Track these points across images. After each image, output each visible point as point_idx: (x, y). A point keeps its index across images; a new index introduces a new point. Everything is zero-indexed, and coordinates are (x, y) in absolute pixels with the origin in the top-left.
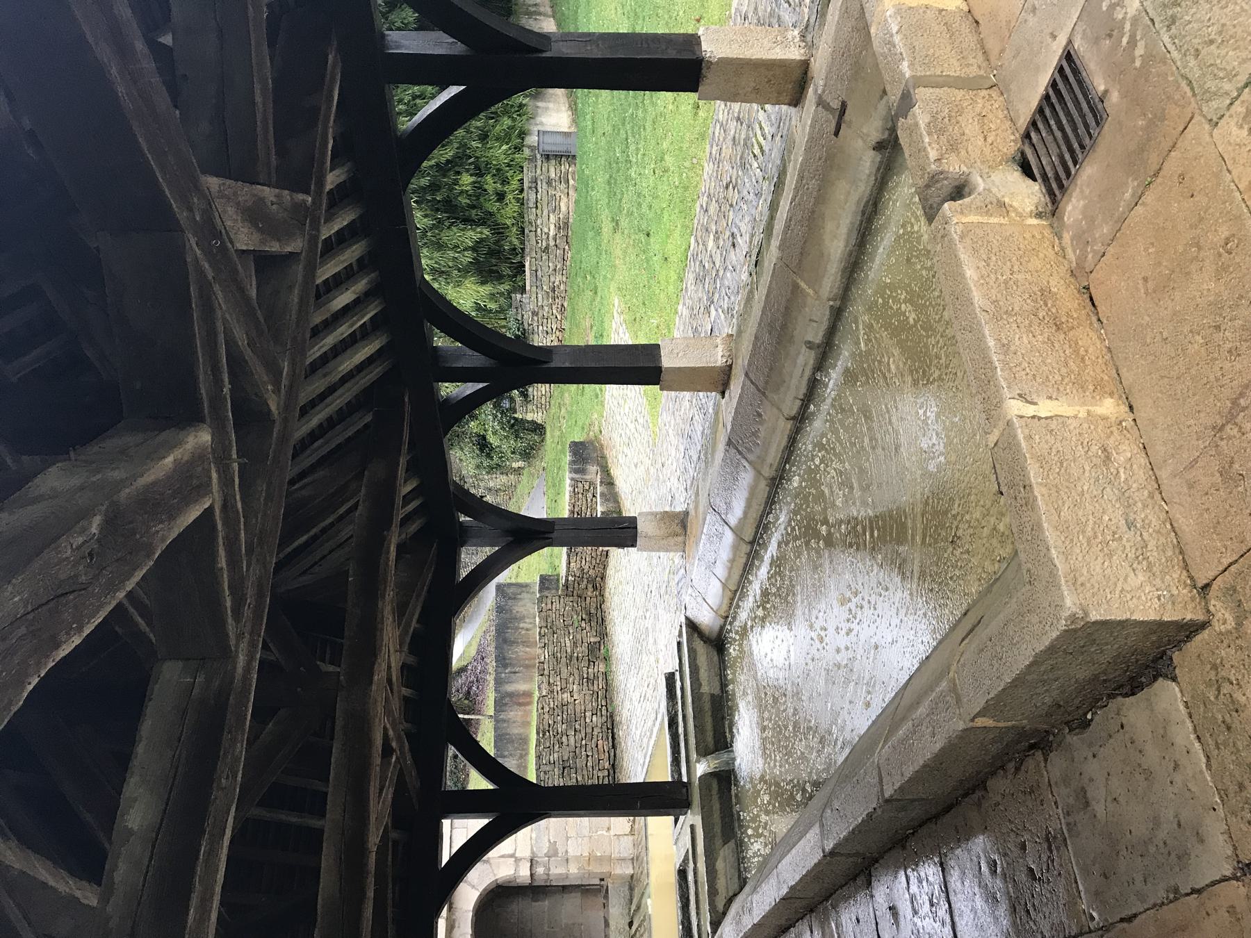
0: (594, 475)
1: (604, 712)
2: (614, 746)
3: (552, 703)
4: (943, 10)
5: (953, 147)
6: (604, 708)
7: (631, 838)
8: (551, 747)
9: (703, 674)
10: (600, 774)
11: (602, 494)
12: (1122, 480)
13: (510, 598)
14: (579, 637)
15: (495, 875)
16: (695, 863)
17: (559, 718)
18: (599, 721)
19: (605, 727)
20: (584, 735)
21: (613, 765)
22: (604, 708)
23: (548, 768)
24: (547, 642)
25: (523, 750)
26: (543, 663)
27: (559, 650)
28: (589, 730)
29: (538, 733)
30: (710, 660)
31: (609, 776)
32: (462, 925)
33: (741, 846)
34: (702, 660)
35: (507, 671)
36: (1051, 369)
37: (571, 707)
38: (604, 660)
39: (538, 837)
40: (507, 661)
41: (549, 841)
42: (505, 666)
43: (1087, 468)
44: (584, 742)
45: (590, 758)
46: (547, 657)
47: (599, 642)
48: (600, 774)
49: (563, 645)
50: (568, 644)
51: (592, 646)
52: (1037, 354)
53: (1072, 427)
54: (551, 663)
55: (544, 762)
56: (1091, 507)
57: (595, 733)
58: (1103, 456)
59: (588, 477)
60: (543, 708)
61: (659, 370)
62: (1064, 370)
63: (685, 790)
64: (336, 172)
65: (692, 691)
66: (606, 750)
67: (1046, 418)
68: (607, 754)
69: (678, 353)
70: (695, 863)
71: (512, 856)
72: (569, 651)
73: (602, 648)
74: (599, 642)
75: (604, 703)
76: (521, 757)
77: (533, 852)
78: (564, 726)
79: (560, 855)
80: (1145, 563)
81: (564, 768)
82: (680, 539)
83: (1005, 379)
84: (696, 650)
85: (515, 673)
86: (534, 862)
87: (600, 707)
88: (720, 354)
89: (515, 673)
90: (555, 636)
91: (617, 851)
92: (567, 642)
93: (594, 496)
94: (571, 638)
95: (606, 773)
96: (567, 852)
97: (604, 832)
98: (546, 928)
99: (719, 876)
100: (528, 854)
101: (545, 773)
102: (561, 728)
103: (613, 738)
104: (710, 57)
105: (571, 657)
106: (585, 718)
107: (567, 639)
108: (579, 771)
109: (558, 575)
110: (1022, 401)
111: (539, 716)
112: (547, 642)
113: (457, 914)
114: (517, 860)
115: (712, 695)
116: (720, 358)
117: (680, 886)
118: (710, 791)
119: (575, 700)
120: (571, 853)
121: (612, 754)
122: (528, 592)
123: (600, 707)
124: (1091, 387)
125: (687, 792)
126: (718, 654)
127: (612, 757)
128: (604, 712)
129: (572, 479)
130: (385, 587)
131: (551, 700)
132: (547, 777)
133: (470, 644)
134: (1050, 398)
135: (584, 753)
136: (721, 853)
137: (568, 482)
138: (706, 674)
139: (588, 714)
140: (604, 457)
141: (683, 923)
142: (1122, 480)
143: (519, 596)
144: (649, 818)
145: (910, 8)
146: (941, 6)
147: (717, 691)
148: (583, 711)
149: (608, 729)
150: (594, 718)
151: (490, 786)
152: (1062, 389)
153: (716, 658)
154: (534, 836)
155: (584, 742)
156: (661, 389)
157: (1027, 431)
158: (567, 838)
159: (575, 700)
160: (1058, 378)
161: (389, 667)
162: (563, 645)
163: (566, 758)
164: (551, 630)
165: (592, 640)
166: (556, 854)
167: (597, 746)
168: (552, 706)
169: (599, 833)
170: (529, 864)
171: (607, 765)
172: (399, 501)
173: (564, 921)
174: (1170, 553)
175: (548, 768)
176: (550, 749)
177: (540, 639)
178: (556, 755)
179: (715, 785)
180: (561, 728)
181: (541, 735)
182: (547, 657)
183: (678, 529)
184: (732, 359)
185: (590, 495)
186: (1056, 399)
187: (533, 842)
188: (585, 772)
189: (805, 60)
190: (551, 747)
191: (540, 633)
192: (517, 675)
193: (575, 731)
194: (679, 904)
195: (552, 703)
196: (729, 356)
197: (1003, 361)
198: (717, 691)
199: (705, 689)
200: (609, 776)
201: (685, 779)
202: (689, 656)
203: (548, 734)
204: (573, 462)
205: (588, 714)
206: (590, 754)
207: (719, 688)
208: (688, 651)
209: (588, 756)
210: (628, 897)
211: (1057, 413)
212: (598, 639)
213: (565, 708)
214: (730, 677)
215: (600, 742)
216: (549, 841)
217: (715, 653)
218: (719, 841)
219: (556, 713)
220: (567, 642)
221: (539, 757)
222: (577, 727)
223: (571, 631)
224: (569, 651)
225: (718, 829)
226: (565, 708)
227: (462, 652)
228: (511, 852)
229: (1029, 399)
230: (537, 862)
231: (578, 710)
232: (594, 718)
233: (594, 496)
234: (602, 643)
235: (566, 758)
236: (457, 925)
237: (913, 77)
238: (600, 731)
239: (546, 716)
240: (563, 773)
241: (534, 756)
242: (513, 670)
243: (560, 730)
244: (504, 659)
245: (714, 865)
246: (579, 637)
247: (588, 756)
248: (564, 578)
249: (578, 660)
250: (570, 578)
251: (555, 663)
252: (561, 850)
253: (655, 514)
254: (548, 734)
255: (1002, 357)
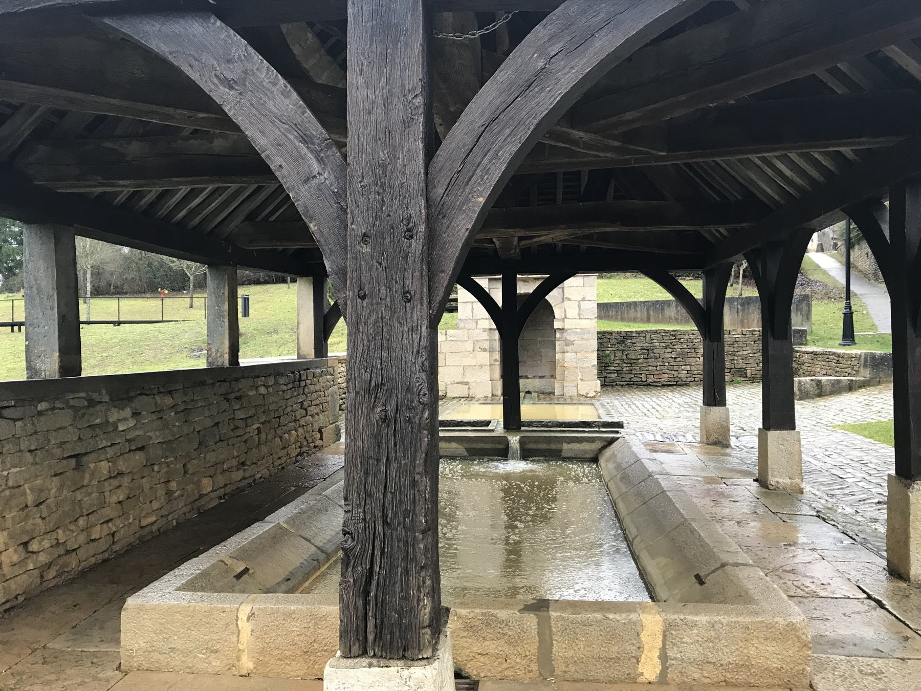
0: (864, 375)
1: (689, 379)
2: (663, 386)
3: (697, 341)
4: (638, 662)
5: (469, 627)
6: (693, 379)
7: (576, 394)
8: (663, 341)
9: (576, 446)
10: (643, 375)
11: (839, 381)
12: (198, 655)
13: (797, 305)
14: (751, 361)
15: (555, 306)
16: (471, 431)
17: (685, 346)
18: (683, 376)
19: (678, 379)
20: (671, 364)
21: (650, 385)
22: (693, 379)
23: (648, 338)
24: (747, 336)
25: (681, 320)
26: (729, 333)
27: (739, 345)
28: (675, 368)
29: (674, 331)
30: (585, 452)
31: (642, 381)
32: (526, 287)
33: (452, 459)
34: (586, 446)
35: (739, 306)
36: (273, 638)
37: (694, 355)
38: (731, 380)
39: (577, 333)
40: (746, 306)
41: (574, 341)
42: (743, 305)
43: (205, 637)
44: (667, 364)
45: (655, 368)
46: (734, 336)
47: (747, 377)
48: (643, 375)
49: (744, 349)
50: (745, 353)
51: (743, 371)
52: (284, 633)
53: (231, 637)
54: (729, 339)
55: (652, 336)
56: (182, 632)
57: (673, 372)
58: (213, 649)
59: (862, 369)
60: (693, 334)
61: (769, 429)
62: (273, 646)
63: (515, 428)
64: (850, 153)
65: (564, 437)
66: (661, 380)
67: (237, 624)
68: (658, 380)
69: (783, 445)
70: (471, 431)
71: (566, 317)
72: (739, 353)
73: (742, 379)
74: (747, 377)
75: (696, 379)
76: (676, 319)
77: (567, 330)
78: (679, 350)
79: (565, 347)
80: (150, 649)
81: (648, 350)
82: (705, 441)
83: (266, 608)
84: (594, 442)
85: (738, 312)
86: (562, 331)
87: (693, 376)
88: (781, 480)
89: (738, 312)
90: (752, 343)
91: (568, 385)
92: (747, 352)
93: (849, 374)
94: (750, 355)
95: (644, 379)
96: (567, 352)
97: (580, 377)
98: (540, 339)
99: (447, 444)
100: (566, 327)
101: (645, 337)
102: (678, 348)
103: (670, 385)
104: (913, 488)
105: (734, 355)
106: (685, 365)
107: (749, 352)
108: (645, 361)
109: (806, 344)
110: (249, 613)
111: (687, 331)
112: (747, 336)
113: (532, 283)
114: (563, 320)
115: (561, 451)
116: (777, 480)
117: (483, 422)
118: (498, 443)
119: (699, 358)
120: (566, 354)
121: (658, 384)
122: (802, 320)
123: (693, 376)
124: (261, 658)
125: (514, 429)
126: (591, 458)
127: (655, 384)
128: (689, 379)
129: (860, 356)
130: (576, 228)
131: (699, 340)
132: (642, 338)
133: (825, 272)
134: (252, 631)
135: (659, 364)
136: (461, 447)
137: (859, 352)
138: (576, 448)
139: (688, 368)
140: (879, 383)
141: (461, 422)
142: (198, 655)
143: (799, 313)
144: (502, 405)
145: (638, 635)
146: (643, 659)
147: (564, 454)
148: (690, 364)
149: (677, 382)
150: (685, 372)
151: (500, 304)
152: (259, 640)
153: (588, 456)
154: (578, 330)
155: (667, 364)
156: (759, 429)
157: (228, 610)
158: (576, 353)
159: (699, 358)
160: (267, 640)
161: (539, 236)
162: (744, 349)
163: (655, 351)
164: (757, 339)
165: (749, 371)
166: (567, 345)
167: (663, 373)
168: (695, 341)
169: (579, 373)
170: (561, 328)
171: (650, 380)
172: (707, 228)
173: (543, 350)
174: (156, 665)
175: (648, 338)
176: (660, 341)
177: (750, 331)
178: (657, 344)
179: (501, 446)
180: (678, 348)
181: (672, 333)
182: (734, 336)
183: (713, 438)
184: (775, 490)
185: (849, 370)
186: (252, 635)
187: (574, 330)
188: (645, 365)
189: (910, 578)
190: (663, 341)
191: (755, 331)
192: (736, 314)
193: (675, 358)
194: (472, 421)
195: (697, 341)
196: (779, 488)
197: (279, 611)
198: (564, 454)
199: (565, 446)
200: (642, 381)
201: (523, 428)
202: (589, 437)
203: (673, 338)
204: (873, 356)
205: (688, 368)
206: (658, 368)
207: (566, 456)
208: (593, 437)
209: (656, 367)
210: (545, 391)
211: (241, 632)
212: (749, 375)
213: (693, 350)
214: (551, 463)
215: (666, 376)
216: (574, 341)
217: (592, 456)
218: (467, 445)
219: (689, 344)
220: (747, 352)
221: (656, 332)
222: (678, 359)
223: (756, 355)
224: (739, 353)
225: (474, 446)
226: (693, 350)
227: (823, 267)
228: (567, 316)
229: (251, 618)
230: (563, 333)
231: (691, 360)
232: (685, 372)
233: (849, 374)
234: (745, 379)
235: (655, 351)
236: (526, 283)
237: (550, 617)
238: (675, 376)
239: (687, 337)
240: (644, 349)
241: (657, 329)
242: (739, 311)
243: (676, 347)
244: (748, 304)
245: (454, 441)
246: (751, 361)
247: (656, 367)
248: (799, 349)
249: (732, 360)
250: (798, 354)
251: (729, 343)
252: (569, 348)
253: (727, 420)
254: (673, 338)
255: (281, 611)
